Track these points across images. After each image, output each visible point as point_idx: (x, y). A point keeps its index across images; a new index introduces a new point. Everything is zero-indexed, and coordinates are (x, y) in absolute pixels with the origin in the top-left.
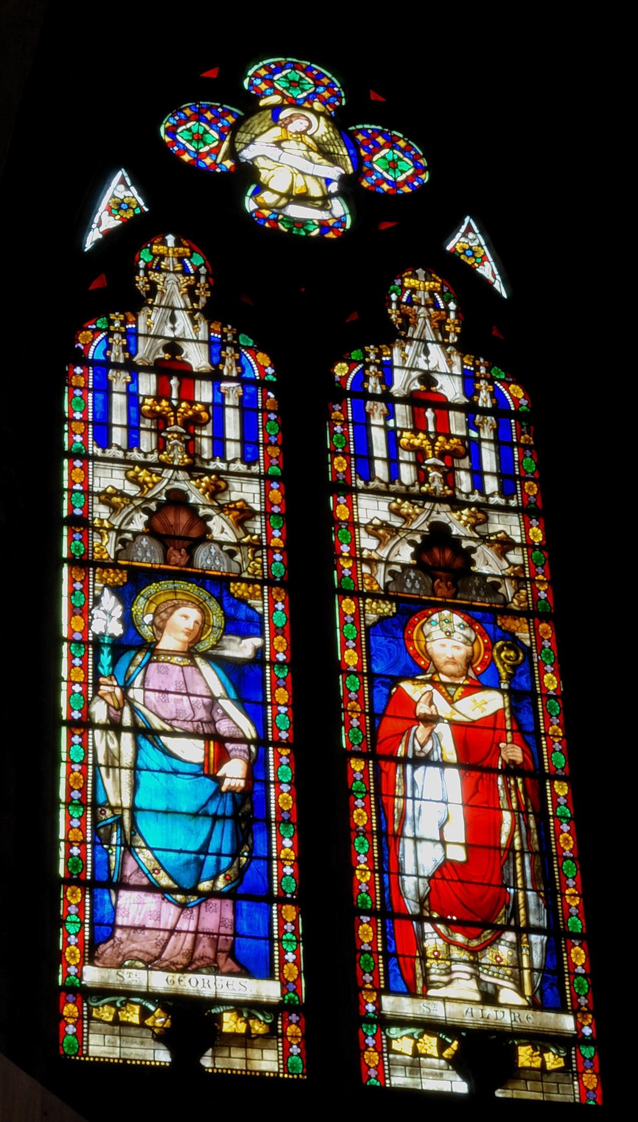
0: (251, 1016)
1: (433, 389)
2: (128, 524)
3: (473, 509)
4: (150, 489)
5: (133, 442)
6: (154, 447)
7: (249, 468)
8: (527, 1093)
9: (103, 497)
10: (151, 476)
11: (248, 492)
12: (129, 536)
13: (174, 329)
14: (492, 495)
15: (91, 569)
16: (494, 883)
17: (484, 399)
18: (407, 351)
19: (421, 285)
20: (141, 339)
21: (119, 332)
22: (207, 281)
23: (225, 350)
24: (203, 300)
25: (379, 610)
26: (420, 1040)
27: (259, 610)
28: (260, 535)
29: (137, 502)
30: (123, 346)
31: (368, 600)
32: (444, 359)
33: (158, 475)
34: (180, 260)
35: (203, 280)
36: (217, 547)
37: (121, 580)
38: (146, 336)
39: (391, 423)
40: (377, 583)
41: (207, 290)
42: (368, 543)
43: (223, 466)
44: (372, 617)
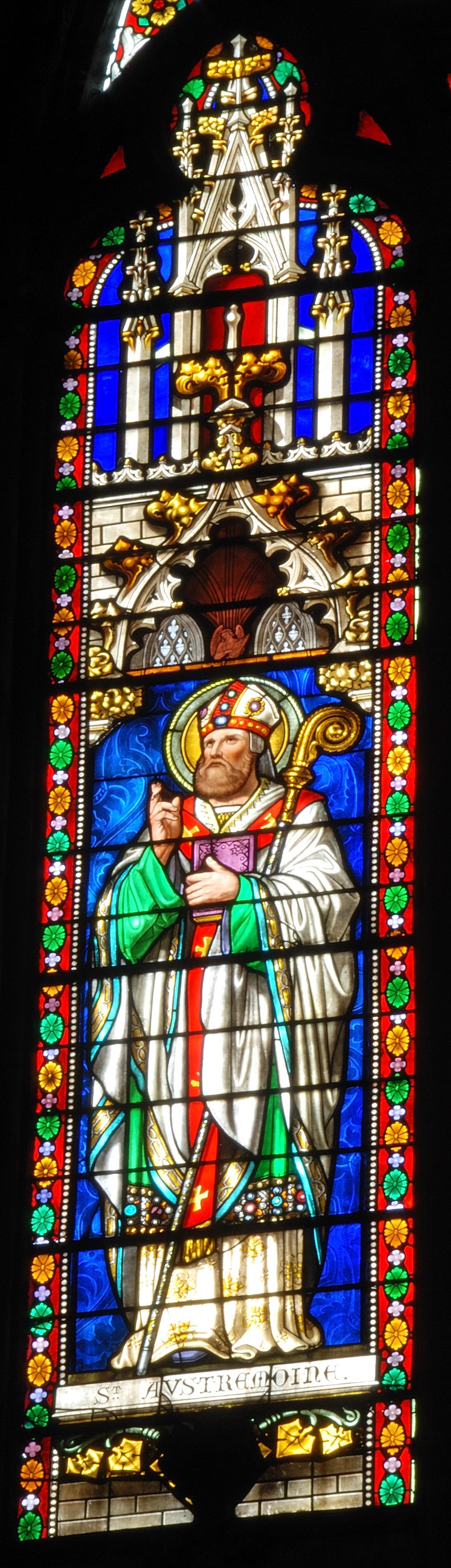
1: (245, 267)
2: (149, 601)
4: (186, 528)
5: (159, 447)
6: (193, 447)
8: (299, 1499)
9: (108, 563)
10: (187, 504)
11: (349, 492)
12: (150, 622)
13: (237, 215)
14: (328, 441)
17: (330, 266)
20: (183, 248)
22: (297, 111)
24: (288, 149)
26: (115, 1449)
27: (366, 705)
28: (369, 568)
31: (96, 695)
34: (255, 78)
35: (290, 108)
36: (295, 606)
37: (132, 704)
38: (192, 239)
39: (163, 353)
41: (296, 127)
42: (101, 588)
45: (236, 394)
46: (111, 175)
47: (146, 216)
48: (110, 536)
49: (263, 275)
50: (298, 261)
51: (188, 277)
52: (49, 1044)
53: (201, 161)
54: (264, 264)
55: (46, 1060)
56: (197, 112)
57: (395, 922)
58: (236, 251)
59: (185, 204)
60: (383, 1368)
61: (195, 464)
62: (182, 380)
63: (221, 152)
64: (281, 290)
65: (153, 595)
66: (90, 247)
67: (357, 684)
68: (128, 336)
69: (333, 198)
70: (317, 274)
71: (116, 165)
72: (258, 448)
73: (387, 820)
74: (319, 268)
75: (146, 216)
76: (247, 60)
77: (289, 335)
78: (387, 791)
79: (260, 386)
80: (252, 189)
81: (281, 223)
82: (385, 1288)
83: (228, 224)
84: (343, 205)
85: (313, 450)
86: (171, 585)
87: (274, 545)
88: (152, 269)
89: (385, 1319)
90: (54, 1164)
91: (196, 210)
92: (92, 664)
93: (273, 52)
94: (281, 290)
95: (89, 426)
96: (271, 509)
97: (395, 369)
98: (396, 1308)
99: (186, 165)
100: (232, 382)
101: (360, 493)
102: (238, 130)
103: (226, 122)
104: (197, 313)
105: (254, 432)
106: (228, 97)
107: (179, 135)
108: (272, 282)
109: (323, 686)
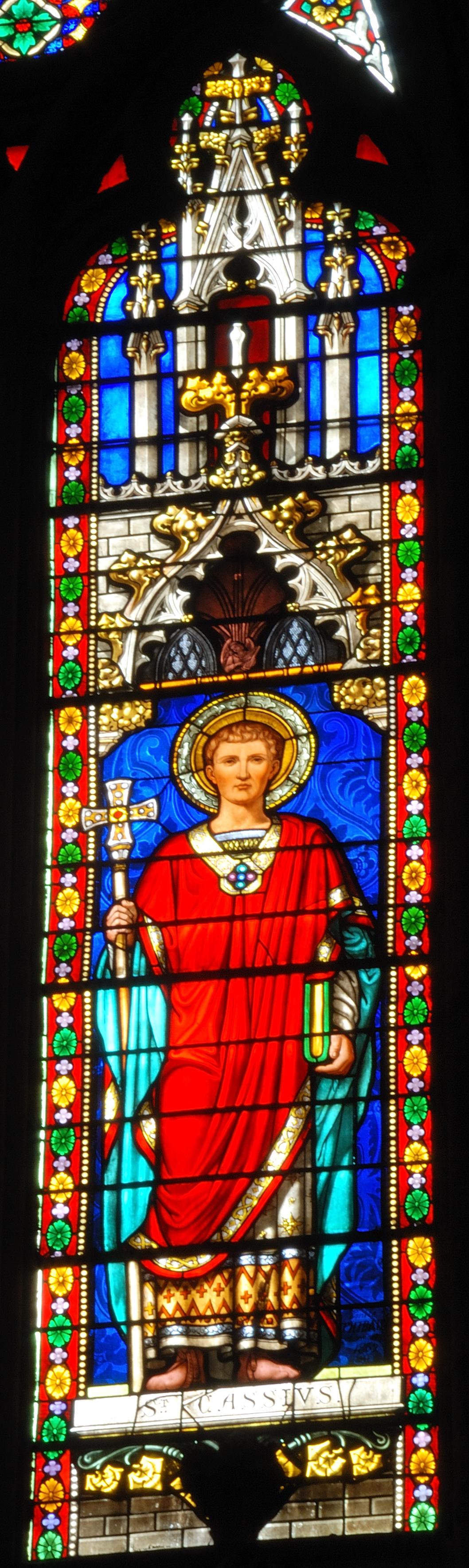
0: (353, 1444)
2: (158, 613)
3: (301, 496)
4: (193, 543)
7: (363, 466)
12: (158, 635)
13: (242, 231)
14: (337, 459)
15: (92, 708)
16: (141, 1179)
18: (206, 218)
19: (237, 88)
20: (187, 266)
21: (146, 262)
23: (330, 254)
25: (121, 721)
27: (382, 724)
29: (170, 571)
30: (155, 287)
32: (272, 218)
33: (206, 513)
40: (120, 673)
42: (110, 601)
43: (319, 473)
44: (108, 738)
45: (243, 411)
46: (110, 190)
47: (149, 227)
48: (117, 547)
49: (268, 294)
50: (305, 280)
51: (193, 291)
52: (71, 380)
53: (202, 174)
54: (271, 282)
55: (69, 350)
56: (197, 128)
57: (413, 941)
58: (241, 265)
59: (189, 216)
60: (408, 1389)
61: (203, 480)
62: (186, 399)
63: (224, 167)
64: (288, 309)
65: (162, 608)
66: (77, 48)
67: (371, 701)
68: (133, 352)
69: (337, 216)
70: (326, 293)
71: (116, 176)
72: (264, 466)
73: (404, 843)
74: (327, 287)
75: (149, 227)
76: (246, 81)
77: (298, 352)
78: (403, 815)
79: (266, 409)
80: (258, 207)
81: (288, 243)
82: (408, 1307)
83: (234, 244)
84: (349, 224)
85: (320, 469)
86: (180, 598)
87: (284, 560)
88: (157, 281)
89: (408, 1339)
90: (73, 1035)
91: (201, 223)
92: (101, 676)
93: (273, 76)
94: (288, 309)
95: (86, 1120)
96: (280, 524)
97: (409, 928)
98: (420, 1328)
99: (185, 180)
100: (238, 401)
101: (370, 511)
102: (241, 147)
103: (228, 138)
104: (201, 330)
105: (260, 447)
106: (227, 116)
107: (177, 149)
108: (279, 302)
109: (338, 704)
